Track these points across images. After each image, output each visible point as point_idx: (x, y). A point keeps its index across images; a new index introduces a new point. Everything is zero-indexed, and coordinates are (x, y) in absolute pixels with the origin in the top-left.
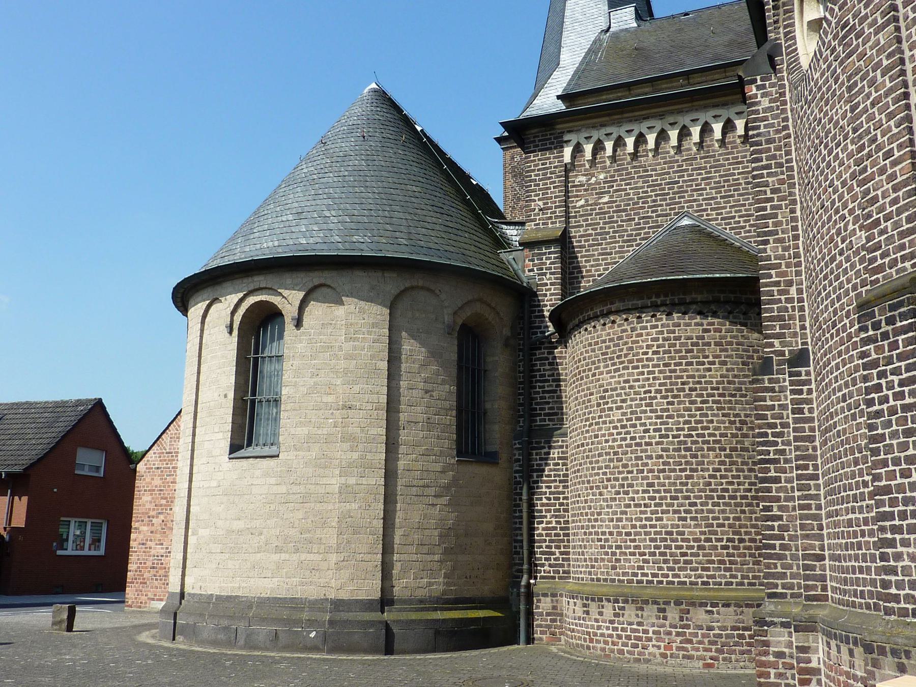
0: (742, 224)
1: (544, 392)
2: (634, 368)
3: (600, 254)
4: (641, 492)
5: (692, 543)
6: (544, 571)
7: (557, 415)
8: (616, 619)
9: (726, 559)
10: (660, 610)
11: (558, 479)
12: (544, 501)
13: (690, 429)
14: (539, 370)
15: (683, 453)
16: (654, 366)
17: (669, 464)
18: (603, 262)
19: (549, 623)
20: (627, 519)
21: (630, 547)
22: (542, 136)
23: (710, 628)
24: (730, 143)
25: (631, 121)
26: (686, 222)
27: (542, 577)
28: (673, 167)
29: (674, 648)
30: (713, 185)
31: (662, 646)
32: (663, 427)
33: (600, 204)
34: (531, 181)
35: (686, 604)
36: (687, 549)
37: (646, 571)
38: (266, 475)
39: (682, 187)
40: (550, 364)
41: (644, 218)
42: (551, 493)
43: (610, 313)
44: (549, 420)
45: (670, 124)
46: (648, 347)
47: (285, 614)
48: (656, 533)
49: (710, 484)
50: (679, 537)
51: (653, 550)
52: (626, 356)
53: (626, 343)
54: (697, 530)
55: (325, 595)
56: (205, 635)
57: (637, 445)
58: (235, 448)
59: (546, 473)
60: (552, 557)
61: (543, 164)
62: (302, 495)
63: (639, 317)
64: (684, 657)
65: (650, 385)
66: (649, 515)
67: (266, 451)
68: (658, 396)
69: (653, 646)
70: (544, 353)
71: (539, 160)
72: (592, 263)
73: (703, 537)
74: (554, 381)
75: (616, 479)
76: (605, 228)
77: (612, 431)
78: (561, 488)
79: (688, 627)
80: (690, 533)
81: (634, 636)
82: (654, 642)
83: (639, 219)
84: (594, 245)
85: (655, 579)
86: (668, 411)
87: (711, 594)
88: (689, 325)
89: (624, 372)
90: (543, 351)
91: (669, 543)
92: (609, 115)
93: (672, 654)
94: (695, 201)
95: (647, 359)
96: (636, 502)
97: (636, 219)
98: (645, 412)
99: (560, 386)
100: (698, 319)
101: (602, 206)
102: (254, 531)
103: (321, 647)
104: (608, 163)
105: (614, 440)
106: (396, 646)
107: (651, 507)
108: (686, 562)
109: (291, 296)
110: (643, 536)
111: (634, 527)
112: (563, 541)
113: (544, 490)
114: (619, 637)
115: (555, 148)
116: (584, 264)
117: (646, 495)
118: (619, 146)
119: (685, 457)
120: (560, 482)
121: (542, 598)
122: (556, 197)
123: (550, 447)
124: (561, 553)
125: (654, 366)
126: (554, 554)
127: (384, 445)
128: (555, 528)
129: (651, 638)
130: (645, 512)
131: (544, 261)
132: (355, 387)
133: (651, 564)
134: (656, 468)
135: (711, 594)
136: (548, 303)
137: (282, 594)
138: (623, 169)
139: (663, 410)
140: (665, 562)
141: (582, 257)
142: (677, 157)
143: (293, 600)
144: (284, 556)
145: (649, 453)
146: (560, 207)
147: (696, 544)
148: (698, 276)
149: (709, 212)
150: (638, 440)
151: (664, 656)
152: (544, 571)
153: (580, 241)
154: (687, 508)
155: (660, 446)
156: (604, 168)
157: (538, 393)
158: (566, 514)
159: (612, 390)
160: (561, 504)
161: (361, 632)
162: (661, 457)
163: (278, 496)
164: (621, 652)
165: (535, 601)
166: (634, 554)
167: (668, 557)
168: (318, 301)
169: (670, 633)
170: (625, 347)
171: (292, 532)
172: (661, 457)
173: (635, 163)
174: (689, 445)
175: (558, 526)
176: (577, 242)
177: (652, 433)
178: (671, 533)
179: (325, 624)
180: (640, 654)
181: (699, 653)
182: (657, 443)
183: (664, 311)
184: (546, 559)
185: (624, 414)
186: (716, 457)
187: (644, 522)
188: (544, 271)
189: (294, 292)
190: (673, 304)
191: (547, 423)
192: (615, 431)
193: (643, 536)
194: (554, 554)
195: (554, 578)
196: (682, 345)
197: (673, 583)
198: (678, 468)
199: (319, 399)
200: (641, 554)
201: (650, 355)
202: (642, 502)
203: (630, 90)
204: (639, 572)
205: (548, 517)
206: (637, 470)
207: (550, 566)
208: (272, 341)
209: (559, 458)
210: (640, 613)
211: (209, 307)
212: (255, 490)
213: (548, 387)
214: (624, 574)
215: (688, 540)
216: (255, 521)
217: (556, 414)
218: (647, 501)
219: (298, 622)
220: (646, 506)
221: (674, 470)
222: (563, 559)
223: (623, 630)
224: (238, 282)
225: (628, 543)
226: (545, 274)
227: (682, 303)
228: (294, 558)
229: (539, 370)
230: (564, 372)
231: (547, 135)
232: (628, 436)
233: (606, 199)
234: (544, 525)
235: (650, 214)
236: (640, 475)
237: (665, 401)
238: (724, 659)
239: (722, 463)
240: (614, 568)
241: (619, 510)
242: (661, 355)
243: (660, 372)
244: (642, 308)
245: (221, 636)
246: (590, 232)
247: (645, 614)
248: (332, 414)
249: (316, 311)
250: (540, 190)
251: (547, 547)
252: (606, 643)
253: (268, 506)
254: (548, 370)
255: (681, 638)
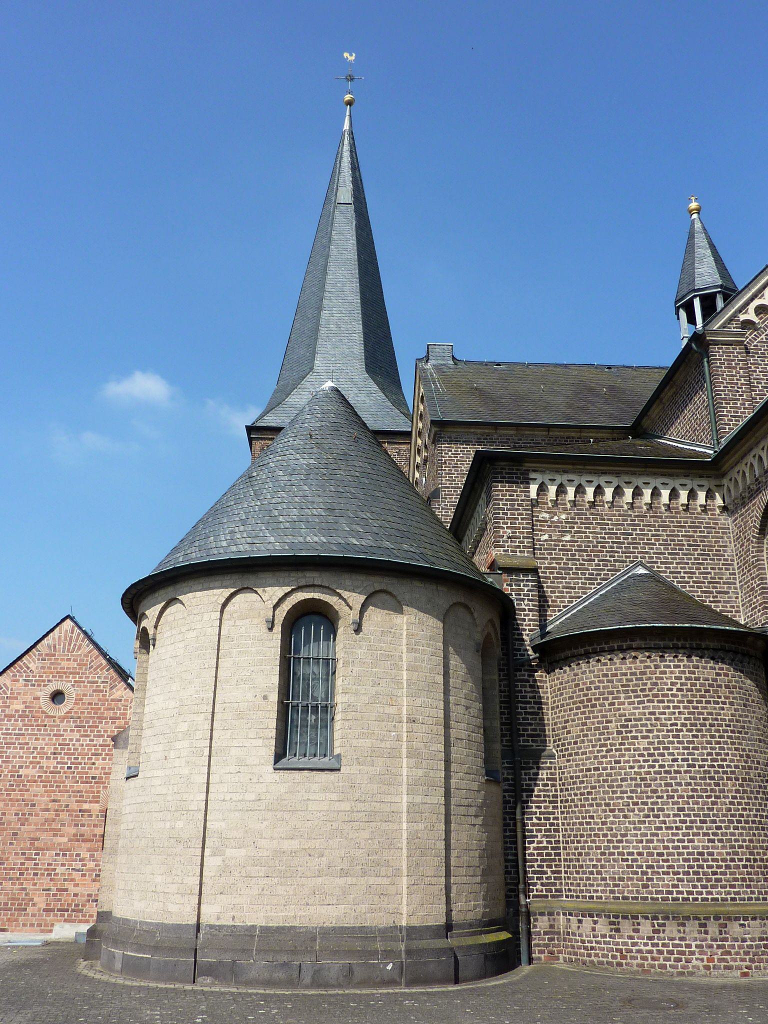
0: (686, 579)
1: (526, 713)
2: (659, 702)
3: (564, 587)
4: (671, 816)
5: (720, 863)
6: (537, 890)
7: (540, 736)
8: (656, 935)
9: (747, 877)
10: (701, 925)
11: (547, 799)
12: (535, 821)
13: (712, 760)
14: (521, 692)
15: (708, 781)
16: (679, 702)
17: (696, 791)
18: (568, 595)
19: (547, 942)
20: (658, 841)
21: (663, 867)
22: (509, 469)
23: (744, 940)
24: (674, 508)
25: (591, 473)
26: (641, 571)
27: (534, 896)
28: (627, 520)
29: (716, 960)
30: (661, 542)
31: (705, 959)
32: (690, 757)
33: (562, 541)
34: (499, 509)
35: (724, 919)
36: (717, 868)
37: (681, 889)
38: (325, 790)
39: (635, 539)
40: (531, 686)
41: (603, 560)
42: (541, 813)
43: (630, 648)
44: (532, 741)
45: (625, 482)
46: (673, 684)
47: (358, 945)
48: (688, 854)
49: (730, 810)
50: (710, 858)
51: (686, 869)
52: (650, 690)
53: (650, 678)
54: (724, 851)
55: (394, 922)
56: (253, 974)
57: (666, 772)
58: (279, 756)
59: (536, 793)
60: (544, 876)
61: (510, 495)
62: (367, 813)
63: (662, 656)
64: (726, 968)
65: (676, 719)
66: (681, 837)
67: (317, 762)
68: (684, 729)
69: (697, 959)
70: (524, 675)
71: (507, 491)
72: (557, 594)
73: (728, 857)
74: (535, 703)
75: (646, 804)
76: (568, 564)
77: (637, 758)
78: (551, 808)
79: (726, 940)
80: (719, 854)
81: (677, 951)
82: (697, 956)
83: (599, 561)
84: (558, 578)
85: (691, 897)
86: (694, 743)
87: (740, 908)
88: (705, 668)
89: (648, 704)
90: (523, 673)
91: (701, 862)
92: (573, 464)
93: (714, 966)
94: (647, 553)
95: (672, 695)
96: (668, 825)
97: (596, 561)
98: (673, 743)
99: (542, 709)
100: (711, 664)
101: (564, 543)
102: (312, 853)
103: (398, 980)
104: (569, 506)
105: (641, 767)
106: (461, 975)
107: (682, 829)
108: (717, 880)
109: (352, 599)
110: (676, 857)
111: (666, 848)
112: (555, 860)
113: (534, 810)
114: (660, 952)
115: (522, 483)
116: (549, 594)
117: (677, 819)
118: (579, 493)
119: (710, 785)
120: (550, 802)
121: (539, 917)
122: (523, 528)
123: (539, 768)
124: (553, 872)
125: (679, 702)
126: (546, 873)
127: (443, 762)
128: (546, 848)
129: (695, 951)
130: (677, 835)
131: (522, 587)
132: (418, 699)
133: (686, 883)
134: (685, 794)
135: (740, 908)
136: (527, 628)
137: (349, 922)
138: (582, 514)
139: (689, 742)
140: (699, 880)
141: (547, 587)
142: (630, 512)
143: (362, 929)
144: (350, 880)
145: (679, 781)
146: (528, 538)
147: (724, 864)
148: (714, 627)
149: (659, 565)
150: (667, 768)
151: (707, 968)
152: (537, 890)
153: (546, 573)
154: (715, 831)
155: (688, 775)
156: (565, 509)
157: (521, 714)
158: (557, 834)
159: (635, 720)
160: (552, 824)
161: (435, 961)
162: (690, 784)
163: (341, 814)
164: (663, 967)
165: (532, 920)
166: (668, 873)
167: (701, 876)
168: (376, 606)
169: (711, 947)
170: (649, 682)
171: (358, 853)
172: (690, 784)
173: (592, 511)
174: (713, 774)
175: (550, 846)
176: (542, 572)
177: (680, 763)
178: (702, 854)
179: (401, 954)
180: (683, 967)
181: (737, 964)
182: (686, 772)
183: (684, 654)
184: (538, 878)
185: (650, 743)
186: (733, 786)
187: (676, 844)
188: (522, 597)
189: (354, 594)
190: (692, 648)
191: (531, 743)
192: (641, 759)
193: (676, 857)
194: (546, 873)
195: (547, 896)
196: (702, 685)
197: (707, 899)
198: (704, 794)
199: (381, 710)
200: (675, 873)
201: (674, 692)
202: (674, 825)
203: (496, 429)
204: (674, 890)
205: (539, 837)
206: (667, 796)
207: (542, 884)
208: (307, 641)
209: (548, 779)
210: (682, 929)
211: (232, 595)
212: (312, 806)
213: (530, 708)
214: (657, 892)
215: (716, 860)
216: (314, 841)
217: (539, 736)
218: (678, 824)
219: (374, 954)
220: (677, 828)
221: (702, 797)
222: (555, 878)
223: (664, 945)
224: (283, 574)
225: (661, 863)
226: (523, 600)
227: (698, 648)
228: (362, 882)
229: (521, 692)
230: (545, 696)
231: (513, 469)
232: (657, 764)
233: (568, 538)
234: (535, 845)
235: (608, 558)
236: (670, 800)
237: (690, 734)
238: (756, 968)
239: (737, 791)
240: (645, 886)
241: (649, 832)
242: (685, 693)
243: (685, 707)
244: (664, 648)
245: (280, 975)
246: (554, 565)
247: (687, 930)
248: (395, 726)
249: (376, 617)
250: (508, 518)
251: (539, 866)
252: (646, 959)
253: (329, 824)
254: (529, 692)
255: (721, 950)
